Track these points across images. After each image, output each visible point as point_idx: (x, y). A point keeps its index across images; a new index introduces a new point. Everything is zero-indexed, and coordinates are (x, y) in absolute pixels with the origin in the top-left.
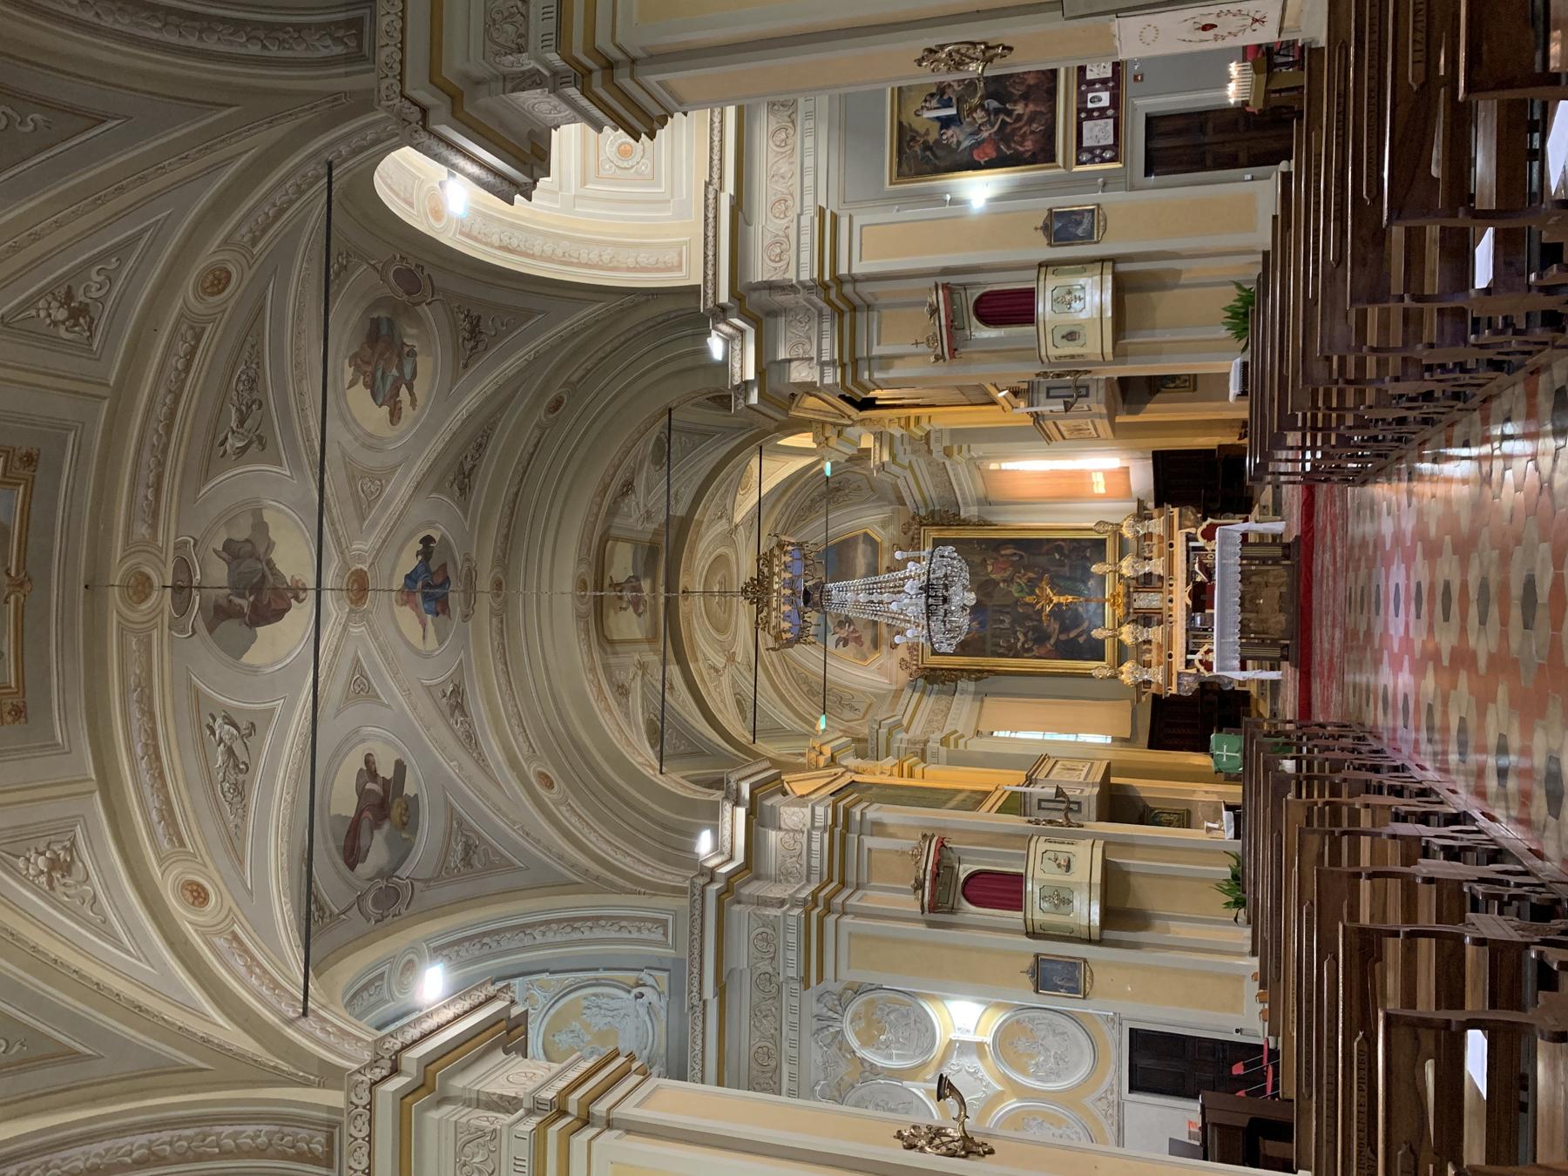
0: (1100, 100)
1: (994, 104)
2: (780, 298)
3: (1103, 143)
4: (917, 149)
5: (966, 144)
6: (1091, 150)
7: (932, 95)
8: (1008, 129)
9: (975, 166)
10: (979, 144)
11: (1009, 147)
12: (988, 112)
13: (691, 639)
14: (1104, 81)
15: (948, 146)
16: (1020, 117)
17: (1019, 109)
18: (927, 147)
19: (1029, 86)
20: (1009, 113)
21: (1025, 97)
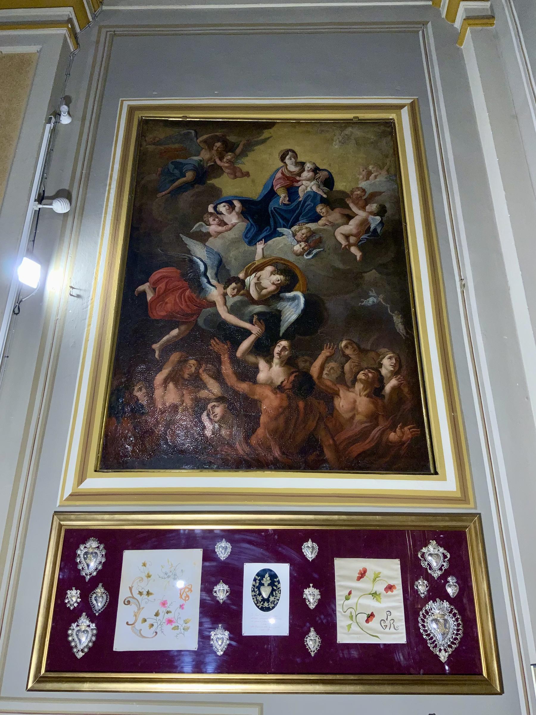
0: (266, 605)
1: (291, 311)
2: (19, 241)
3: (124, 613)
4: (205, 155)
5: (199, 252)
6: (110, 576)
7: (329, 182)
8: (217, 346)
9: (137, 262)
10: (193, 280)
11: (167, 350)
12: (277, 295)
13: (59, 16)
14: (323, 618)
15: (200, 215)
16: (248, 374)
17: (271, 372)
18: (203, 174)
19: (329, 397)
20: (263, 348)
21: (303, 385)
